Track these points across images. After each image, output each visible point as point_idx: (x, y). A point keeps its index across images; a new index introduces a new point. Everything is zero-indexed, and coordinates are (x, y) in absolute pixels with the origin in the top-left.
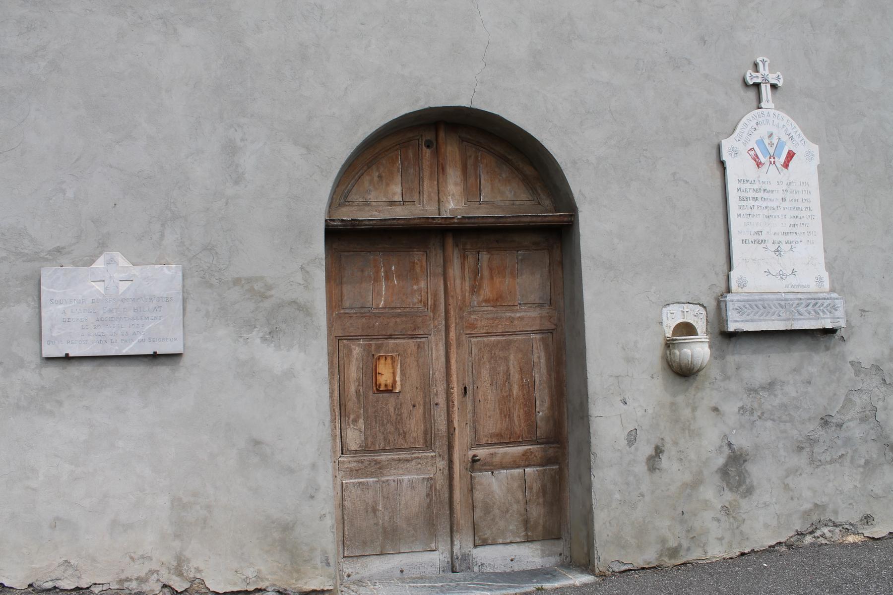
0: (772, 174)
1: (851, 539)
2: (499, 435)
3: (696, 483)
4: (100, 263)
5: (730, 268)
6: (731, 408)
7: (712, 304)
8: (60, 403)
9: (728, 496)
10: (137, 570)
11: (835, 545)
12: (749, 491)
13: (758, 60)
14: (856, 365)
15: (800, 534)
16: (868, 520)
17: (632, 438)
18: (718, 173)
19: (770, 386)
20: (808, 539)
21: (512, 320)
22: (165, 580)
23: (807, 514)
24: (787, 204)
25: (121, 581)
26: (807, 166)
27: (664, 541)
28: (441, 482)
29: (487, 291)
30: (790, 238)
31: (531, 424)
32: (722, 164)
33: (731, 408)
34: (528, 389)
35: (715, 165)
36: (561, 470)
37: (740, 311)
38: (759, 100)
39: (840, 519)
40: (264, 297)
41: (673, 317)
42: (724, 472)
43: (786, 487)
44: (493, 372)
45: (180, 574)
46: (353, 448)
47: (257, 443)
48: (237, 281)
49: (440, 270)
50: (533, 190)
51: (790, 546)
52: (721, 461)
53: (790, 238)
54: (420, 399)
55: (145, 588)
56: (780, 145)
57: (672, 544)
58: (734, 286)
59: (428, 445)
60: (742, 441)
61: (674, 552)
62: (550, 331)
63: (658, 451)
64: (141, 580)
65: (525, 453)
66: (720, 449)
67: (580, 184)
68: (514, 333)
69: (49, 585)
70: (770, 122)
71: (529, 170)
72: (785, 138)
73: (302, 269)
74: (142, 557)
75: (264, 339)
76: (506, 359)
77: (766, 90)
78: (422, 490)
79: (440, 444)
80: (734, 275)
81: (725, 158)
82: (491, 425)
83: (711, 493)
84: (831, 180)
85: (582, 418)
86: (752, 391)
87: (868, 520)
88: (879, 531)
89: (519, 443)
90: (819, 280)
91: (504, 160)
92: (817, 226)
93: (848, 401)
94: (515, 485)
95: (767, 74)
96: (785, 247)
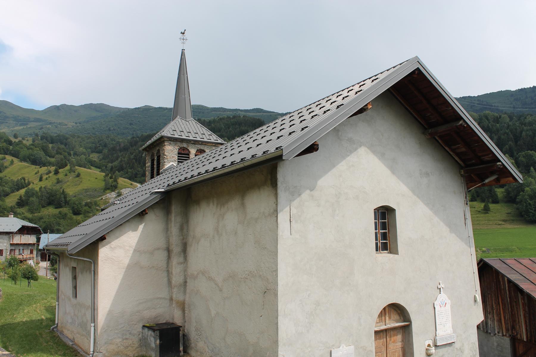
0: (443, 308)
4: (341, 348)
7: (433, 339)
11: (102, 196)
14: (457, 348)
26: (448, 306)
29: (392, 340)
32: (434, 308)
35: (433, 308)
41: (427, 343)
46: (36, 240)
48: (361, 347)
50: (400, 316)
67: (413, 317)
70: (443, 297)
71: (399, 312)
77: (441, 289)
84: (452, 307)
91: (395, 309)
92: (450, 319)
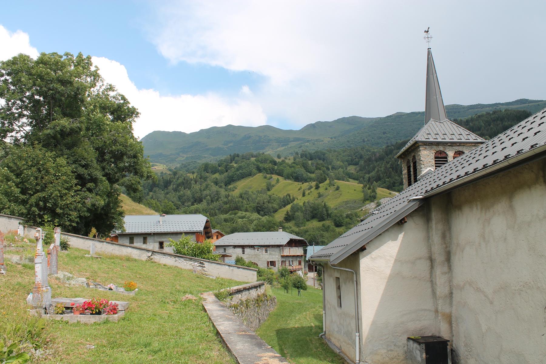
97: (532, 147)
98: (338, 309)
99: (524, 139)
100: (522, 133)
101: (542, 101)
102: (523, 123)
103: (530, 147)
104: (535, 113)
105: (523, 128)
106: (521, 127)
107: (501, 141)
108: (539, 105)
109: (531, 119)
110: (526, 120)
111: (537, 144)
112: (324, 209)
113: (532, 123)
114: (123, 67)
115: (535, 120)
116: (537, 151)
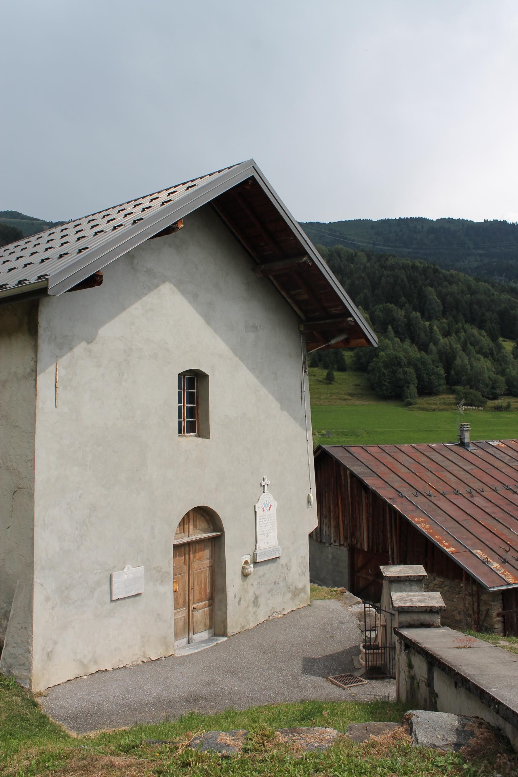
1: (280, 616)
2: (199, 600)
3: (248, 606)
4: (126, 570)
5: (256, 543)
6: (255, 583)
7: (252, 554)
8: (115, 613)
9: (255, 609)
10: (135, 658)
12: (259, 607)
13: (265, 477)
15: (269, 617)
16: (283, 610)
17: (235, 597)
18: (254, 514)
19: (263, 575)
20: (271, 618)
21: (203, 564)
22: (142, 660)
23: (271, 610)
24: (269, 521)
25: (132, 662)
26: (274, 509)
27: (241, 624)
28: (187, 617)
30: (270, 531)
31: (206, 595)
33: (255, 583)
34: (206, 584)
36: (213, 608)
37: (260, 556)
38: (264, 490)
39: (278, 611)
40: (160, 572)
42: (254, 602)
43: (267, 604)
44: (198, 581)
45: (145, 657)
47: (158, 615)
49: (188, 552)
51: (267, 621)
52: (253, 599)
53: (270, 531)
54: (182, 593)
55: (138, 663)
56: (269, 503)
57: (243, 625)
58: (257, 548)
59: (184, 606)
60: (257, 593)
61: (243, 627)
62: (211, 566)
63: (240, 599)
64: (137, 661)
65: (205, 604)
66: (253, 596)
68: (203, 568)
69: (117, 667)
71: (208, 518)
72: (270, 501)
73: (167, 561)
74: (136, 654)
75: (160, 584)
76: (201, 576)
77: (266, 486)
78: (183, 619)
79: (187, 605)
80: (258, 545)
81: (257, 510)
82: (197, 597)
83: (251, 609)
85: (223, 592)
86: (260, 577)
87: (283, 610)
88: (285, 612)
89: (203, 601)
90: (276, 542)
91: (202, 515)
93: (280, 576)
94: (203, 614)
95: (267, 482)
96: (269, 534)
97: (20, 282)
98: (283, 561)
99: (10, 270)
100: (8, 261)
101: (38, 220)
102: (11, 247)
103: (17, 282)
104: (28, 236)
105: (10, 254)
106: (8, 252)
107: (80, 235)
108: (33, 224)
109: (22, 243)
110: (16, 244)
111: (26, 280)
112: (191, 532)
113: (22, 250)
114: (435, 220)
115: (151, 204)
116: (25, 289)
